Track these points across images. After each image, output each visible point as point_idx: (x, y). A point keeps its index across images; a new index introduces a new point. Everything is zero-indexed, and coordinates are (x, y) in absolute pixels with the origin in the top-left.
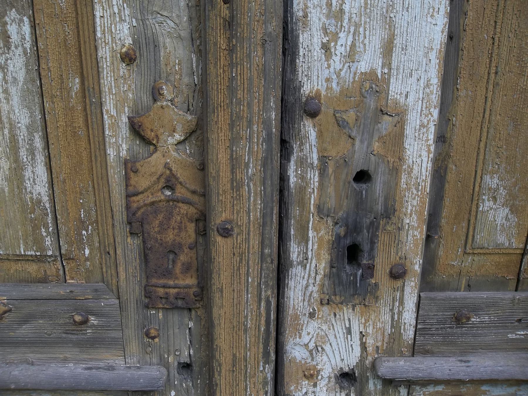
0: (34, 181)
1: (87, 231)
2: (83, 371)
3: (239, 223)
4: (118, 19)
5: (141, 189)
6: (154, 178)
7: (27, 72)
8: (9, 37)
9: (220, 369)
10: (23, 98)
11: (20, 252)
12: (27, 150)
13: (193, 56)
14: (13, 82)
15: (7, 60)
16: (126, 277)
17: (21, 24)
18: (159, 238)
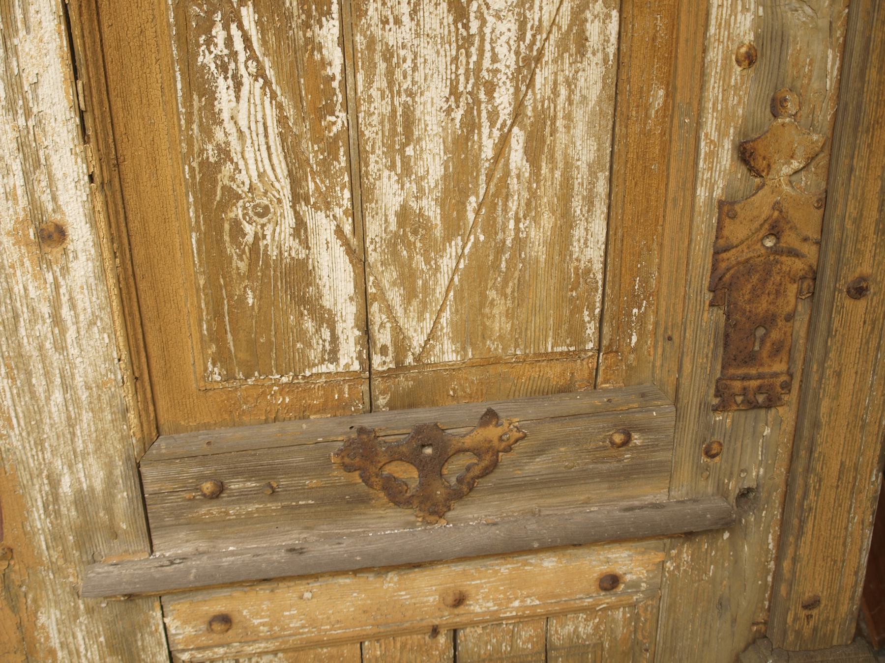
0: (585, 243)
1: (639, 309)
2: (623, 514)
3: (879, 279)
4: (740, 8)
5: (735, 242)
6: (756, 225)
7: (603, 88)
8: (586, 39)
9: (820, 485)
10: (591, 124)
11: (546, 348)
12: (584, 198)
13: (830, 53)
14: (581, 102)
15: (577, 72)
16: (692, 371)
17: (607, 21)
18: (748, 309)
